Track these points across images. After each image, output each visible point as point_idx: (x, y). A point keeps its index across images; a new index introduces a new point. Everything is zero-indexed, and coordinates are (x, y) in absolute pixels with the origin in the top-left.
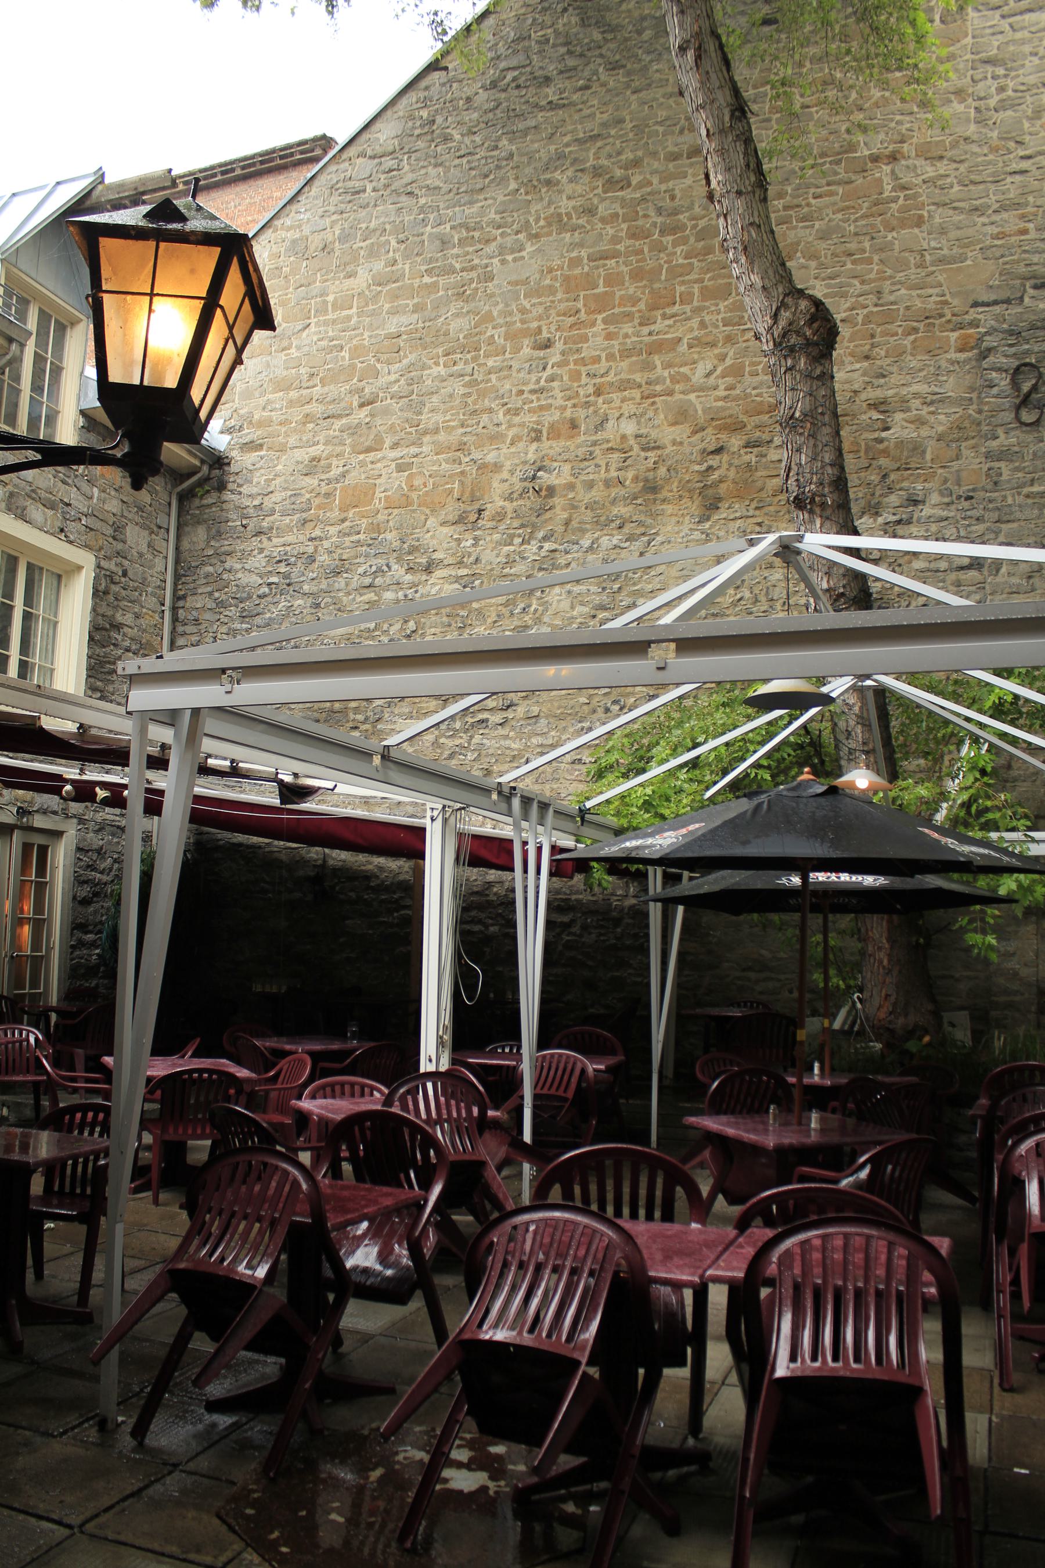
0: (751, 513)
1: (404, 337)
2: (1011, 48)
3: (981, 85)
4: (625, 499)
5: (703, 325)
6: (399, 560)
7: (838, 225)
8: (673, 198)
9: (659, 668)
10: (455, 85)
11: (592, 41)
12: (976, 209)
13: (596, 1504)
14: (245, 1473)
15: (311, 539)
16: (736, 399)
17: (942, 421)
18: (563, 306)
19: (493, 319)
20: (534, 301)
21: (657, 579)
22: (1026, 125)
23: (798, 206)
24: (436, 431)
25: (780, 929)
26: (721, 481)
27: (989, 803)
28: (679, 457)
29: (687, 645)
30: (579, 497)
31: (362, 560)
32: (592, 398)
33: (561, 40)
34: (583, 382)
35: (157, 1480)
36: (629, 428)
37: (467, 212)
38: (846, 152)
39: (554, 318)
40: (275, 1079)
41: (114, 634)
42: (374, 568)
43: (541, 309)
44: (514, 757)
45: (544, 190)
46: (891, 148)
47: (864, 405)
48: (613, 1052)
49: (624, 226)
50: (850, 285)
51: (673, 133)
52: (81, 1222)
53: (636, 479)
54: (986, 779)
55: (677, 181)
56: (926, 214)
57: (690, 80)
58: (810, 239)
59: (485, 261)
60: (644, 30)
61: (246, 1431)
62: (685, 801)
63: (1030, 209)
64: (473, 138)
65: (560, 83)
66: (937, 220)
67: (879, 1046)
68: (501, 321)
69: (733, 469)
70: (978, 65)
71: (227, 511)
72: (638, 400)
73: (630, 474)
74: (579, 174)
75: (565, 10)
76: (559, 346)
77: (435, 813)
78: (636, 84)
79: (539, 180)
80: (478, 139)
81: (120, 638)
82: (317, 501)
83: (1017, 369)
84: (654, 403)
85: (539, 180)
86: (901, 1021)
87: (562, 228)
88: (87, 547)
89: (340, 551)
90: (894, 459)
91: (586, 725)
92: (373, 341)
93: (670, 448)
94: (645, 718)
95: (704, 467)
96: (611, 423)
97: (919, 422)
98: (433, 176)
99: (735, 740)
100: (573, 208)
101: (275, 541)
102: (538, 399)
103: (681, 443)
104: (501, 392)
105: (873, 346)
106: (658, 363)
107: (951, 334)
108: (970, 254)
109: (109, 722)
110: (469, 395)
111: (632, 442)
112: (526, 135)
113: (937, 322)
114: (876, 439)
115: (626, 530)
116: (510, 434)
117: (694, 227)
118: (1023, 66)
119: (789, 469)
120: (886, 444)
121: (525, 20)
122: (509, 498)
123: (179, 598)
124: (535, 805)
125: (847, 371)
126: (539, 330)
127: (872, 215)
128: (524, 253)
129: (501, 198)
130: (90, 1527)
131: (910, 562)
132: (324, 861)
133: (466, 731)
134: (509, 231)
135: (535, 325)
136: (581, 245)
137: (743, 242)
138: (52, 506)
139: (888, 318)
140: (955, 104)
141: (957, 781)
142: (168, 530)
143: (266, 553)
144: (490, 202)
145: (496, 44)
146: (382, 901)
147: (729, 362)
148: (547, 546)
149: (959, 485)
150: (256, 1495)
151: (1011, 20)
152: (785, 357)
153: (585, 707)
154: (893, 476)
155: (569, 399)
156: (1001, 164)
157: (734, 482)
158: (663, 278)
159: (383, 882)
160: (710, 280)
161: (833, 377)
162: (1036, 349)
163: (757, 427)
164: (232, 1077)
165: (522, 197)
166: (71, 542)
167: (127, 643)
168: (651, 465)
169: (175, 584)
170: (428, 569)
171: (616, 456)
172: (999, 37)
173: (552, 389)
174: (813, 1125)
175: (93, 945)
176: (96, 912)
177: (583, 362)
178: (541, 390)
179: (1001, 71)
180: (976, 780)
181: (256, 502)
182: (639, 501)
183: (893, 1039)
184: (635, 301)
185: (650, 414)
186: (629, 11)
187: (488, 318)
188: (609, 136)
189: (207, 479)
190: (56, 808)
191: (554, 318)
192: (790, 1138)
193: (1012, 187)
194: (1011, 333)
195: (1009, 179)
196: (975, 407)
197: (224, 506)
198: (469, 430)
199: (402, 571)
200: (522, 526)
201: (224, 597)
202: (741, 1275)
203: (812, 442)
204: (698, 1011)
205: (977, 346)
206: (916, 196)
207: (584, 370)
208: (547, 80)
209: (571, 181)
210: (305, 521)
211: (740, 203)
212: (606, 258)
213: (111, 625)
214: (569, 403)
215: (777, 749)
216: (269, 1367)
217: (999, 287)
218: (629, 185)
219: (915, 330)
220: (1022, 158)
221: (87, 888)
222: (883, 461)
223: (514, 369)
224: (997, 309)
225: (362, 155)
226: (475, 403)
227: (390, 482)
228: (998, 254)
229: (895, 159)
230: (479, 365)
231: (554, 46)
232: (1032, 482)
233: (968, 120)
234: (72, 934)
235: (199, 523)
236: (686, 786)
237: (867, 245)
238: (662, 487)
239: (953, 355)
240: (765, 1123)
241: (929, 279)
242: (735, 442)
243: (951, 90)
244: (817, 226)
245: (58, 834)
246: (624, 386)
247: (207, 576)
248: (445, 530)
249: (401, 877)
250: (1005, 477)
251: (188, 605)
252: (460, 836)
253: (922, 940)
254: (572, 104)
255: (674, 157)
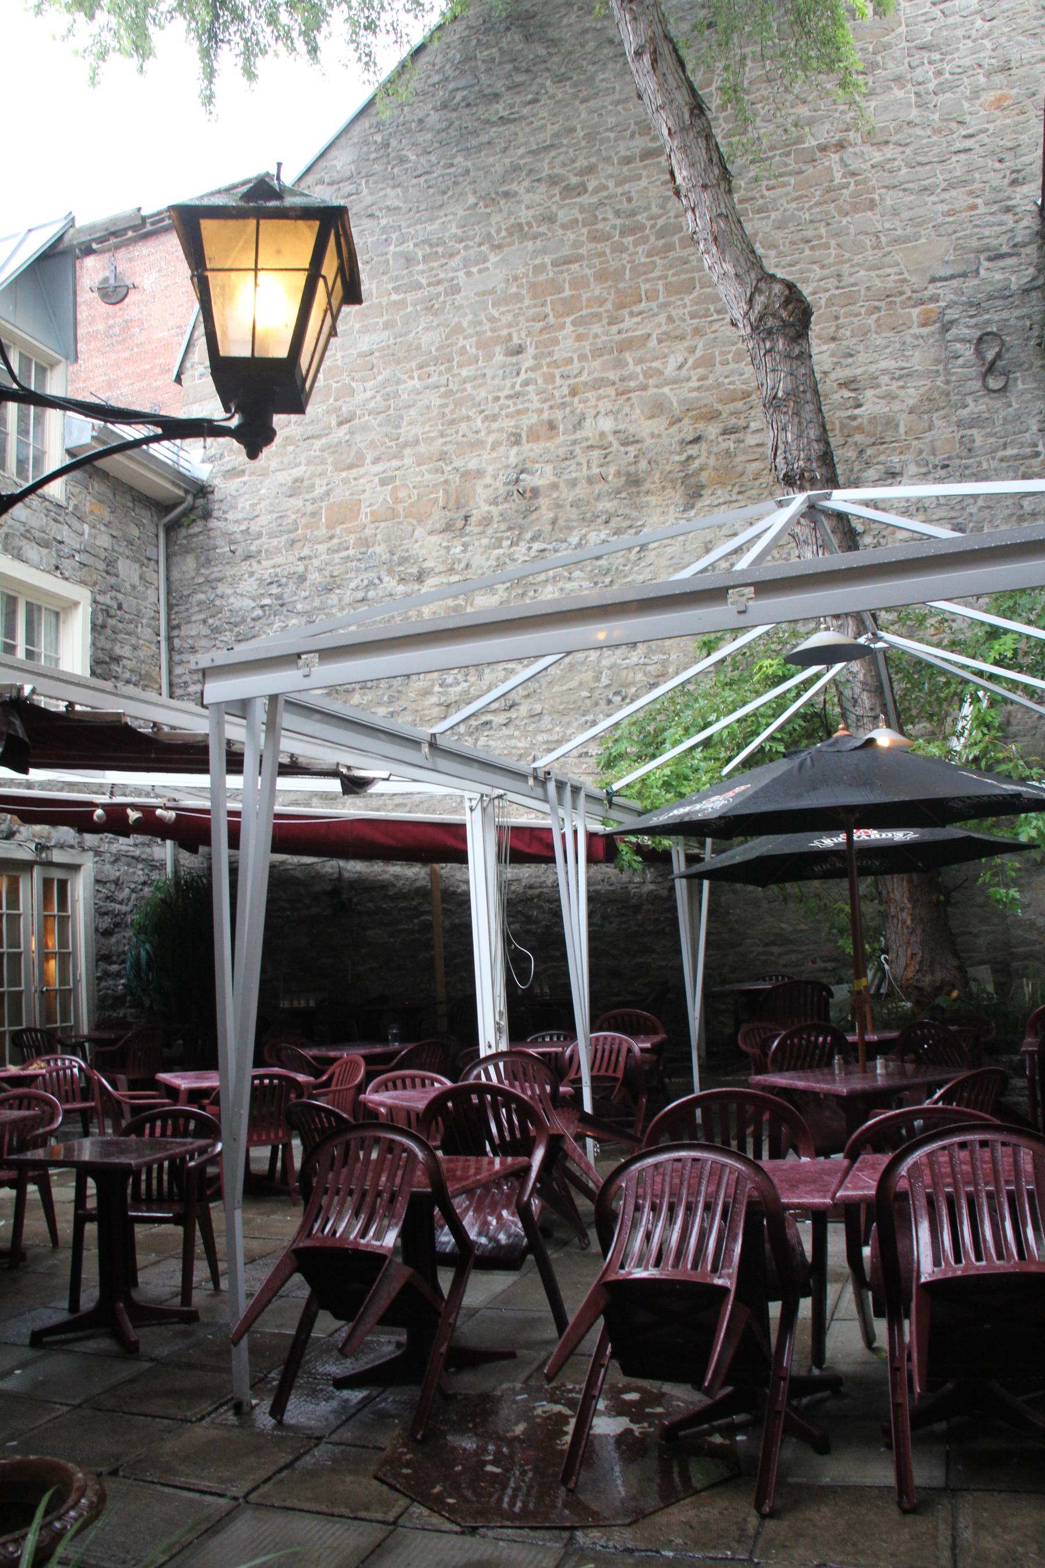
0: (734, 498)
1: (377, 354)
2: (945, 33)
3: (919, 70)
4: (609, 494)
5: (670, 319)
6: (390, 572)
7: (793, 214)
8: (630, 200)
9: (739, 612)
10: (406, 109)
11: (537, 56)
12: (926, 189)
13: (743, 1434)
14: (389, 1439)
15: (301, 559)
16: (708, 388)
17: (912, 395)
18: (531, 312)
19: (463, 330)
20: (502, 309)
21: (648, 570)
22: (966, 105)
23: (752, 199)
24: (416, 443)
25: (801, 901)
26: (702, 470)
27: (1000, 755)
28: (659, 449)
29: (765, 587)
30: (564, 496)
31: (353, 575)
32: (568, 399)
33: (507, 58)
34: (557, 384)
35: (306, 1453)
36: (607, 425)
37: (429, 228)
38: (795, 144)
39: (523, 323)
40: (327, 1084)
41: (114, 667)
42: (366, 582)
43: (509, 317)
44: (521, 756)
45: (502, 202)
46: (837, 137)
47: (835, 385)
48: (654, 1032)
49: (585, 230)
50: (810, 271)
51: (624, 138)
52: (176, 1224)
53: (618, 474)
54: (993, 732)
55: (633, 184)
56: (877, 198)
57: (648, 83)
58: (768, 229)
59: (450, 275)
60: (587, 43)
61: (379, 1403)
62: (704, 779)
63: (977, 185)
64: (428, 157)
65: (508, 98)
66: (889, 202)
67: (909, 1005)
68: (471, 331)
69: (713, 458)
70: (914, 52)
71: (215, 538)
72: (613, 397)
73: (612, 470)
74: (536, 184)
75: (508, 29)
76: (531, 351)
77: (474, 803)
78: (584, 94)
79: (497, 193)
80: (433, 158)
81: (120, 670)
82: (304, 521)
83: (980, 340)
84: (629, 399)
85: (497, 193)
86: (928, 978)
87: (524, 237)
88: (82, 582)
89: (330, 568)
90: (870, 435)
91: (590, 718)
92: (347, 360)
93: (649, 442)
94: (652, 706)
95: (684, 457)
96: (588, 423)
97: (890, 397)
98: (393, 197)
99: (747, 716)
100: (533, 217)
101: (265, 563)
102: (515, 404)
103: (659, 436)
104: (477, 399)
105: (838, 327)
106: (630, 360)
107: (912, 310)
108: (923, 233)
109: (184, 720)
110: (446, 405)
111: (611, 438)
112: (480, 151)
113: (898, 300)
114: (849, 417)
115: (613, 523)
116: (490, 439)
117: (653, 226)
118: (957, 49)
119: (776, 449)
120: (859, 420)
121: (469, 41)
122: (495, 502)
123: (173, 628)
124: (568, 789)
125: (821, 352)
126: (510, 337)
127: (826, 202)
128: (488, 264)
129: (461, 213)
130: (253, 1497)
131: (893, 533)
132: (340, 874)
133: (471, 734)
134: (471, 244)
135: (505, 332)
136: (544, 251)
137: (713, 233)
138: (44, 544)
139: (850, 300)
140: (896, 91)
141: (962, 740)
142: (157, 562)
143: (257, 576)
144: (450, 217)
145: (443, 67)
146: (402, 909)
147: (699, 353)
148: (537, 546)
149: (934, 455)
150: (408, 1457)
151: (941, 6)
152: (763, 340)
153: (587, 701)
154: (869, 452)
155: (545, 401)
156: (945, 145)
157: (715, 469)
158: (627, 277)
159: (400, 890)
160: (673, 275)
161: (810, 356)
162: (996, 318)
163: (732, 414)
164: (295, 1080)
165: (481, 210)
166: (67, 579)
167: (127, 675)
168: (632, 459)
169: (169, 614)
170: (420, 578)
171: (596, 453)
172: (932, 23)
173: (528, 393)
174: (879, 1071)
175: (118, 975)
176: (118, 942)
177: (555, 364)
178: (517, 395)
179: (936, 56)
180: (984, 735)
181: (243, 527)
182: (623, 495)
183: (922, 997)
184: (602, 301)
185: (627, 409)
186: (570, 25)
187: (458, 329)
188: (562, 145)
189: (192, 509)
190: (72, 842)
191: (523, 323)
192: (858, 1084)
193: (957, 165)
194: (971, 305)
195: (955, 158)
196: (942, 378)
197: (211, 534)
198: (448, 439)
199: (394, 583)
200: (510, 529)
201: (218, 623)
202: (873, 1192)
203: (796, 419)
204: (728, 987)
205: (939, 319)
206: (865, 181)
207: (557, 372)
208: (496, 96)
209: (528, 191)
210: (293, 542)
211: (706, 196)
212: (570, 262)
213: (111, 658)
214: (546, 406)
215: (788, 721)
216: (387, 1345)
217: (954, 262)
218: (586, 191)
219: (878, 309)
220: (965, 137)
221: (107, 920)
222: (858, 438)
223: (488, 377)
224: (955, 283)
225: (321, 182)
226: (452, 412)
227: (374, 496)
228: (950, 231)
229: (843, 147)
230: (453, 376)
231: (500, 63)
232: (1005, 446)
233: (909, 105)
234: (97, 966)
235: (187, 552)
236: (702, 764)
237: (823, 231)
238: (645, 480)
239: (916, 330)
240: (833, 1074)
241: (886, 259)
242: (712, 430)
243: (890, 77)
244: (773, 217)
245: (75, 868)
246: (598, 384)
247: (200, 603)
248: (435, 539)
249: (418, 884)
250: (978, 444)
251: (183, 633)
252: (500, 828)
253: (942, 898)
254: (522, 118)
255: (627, 161)
